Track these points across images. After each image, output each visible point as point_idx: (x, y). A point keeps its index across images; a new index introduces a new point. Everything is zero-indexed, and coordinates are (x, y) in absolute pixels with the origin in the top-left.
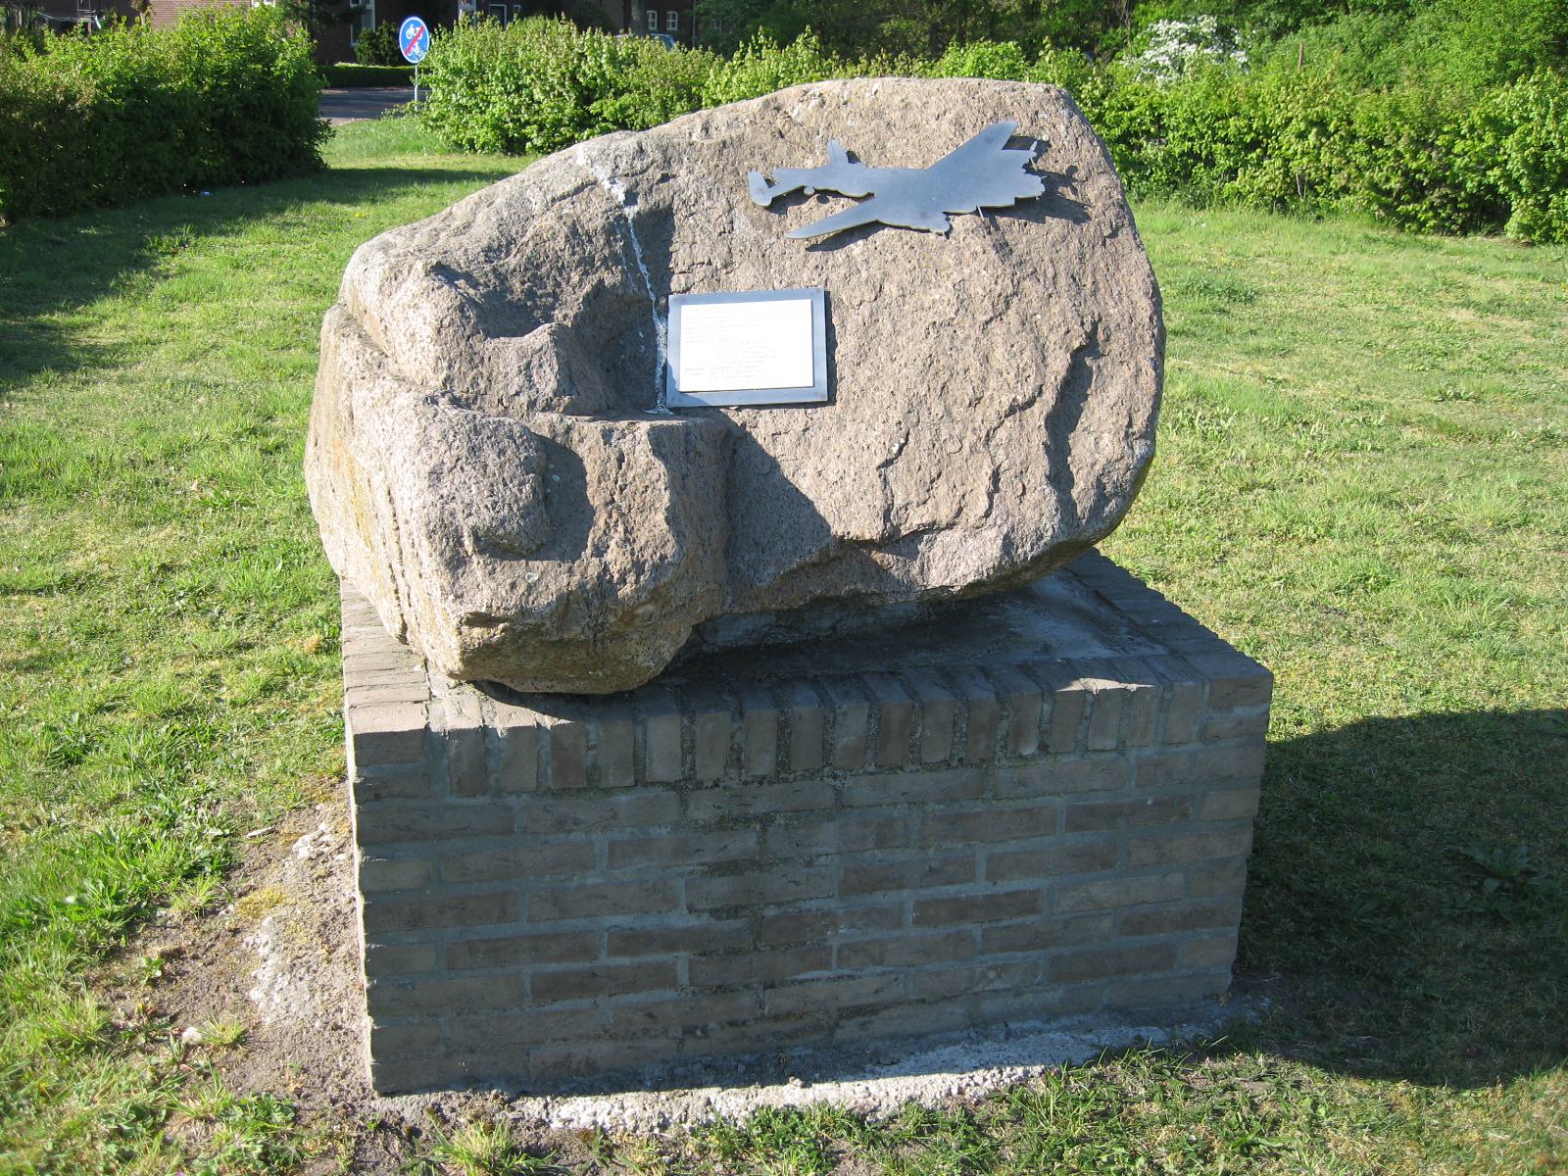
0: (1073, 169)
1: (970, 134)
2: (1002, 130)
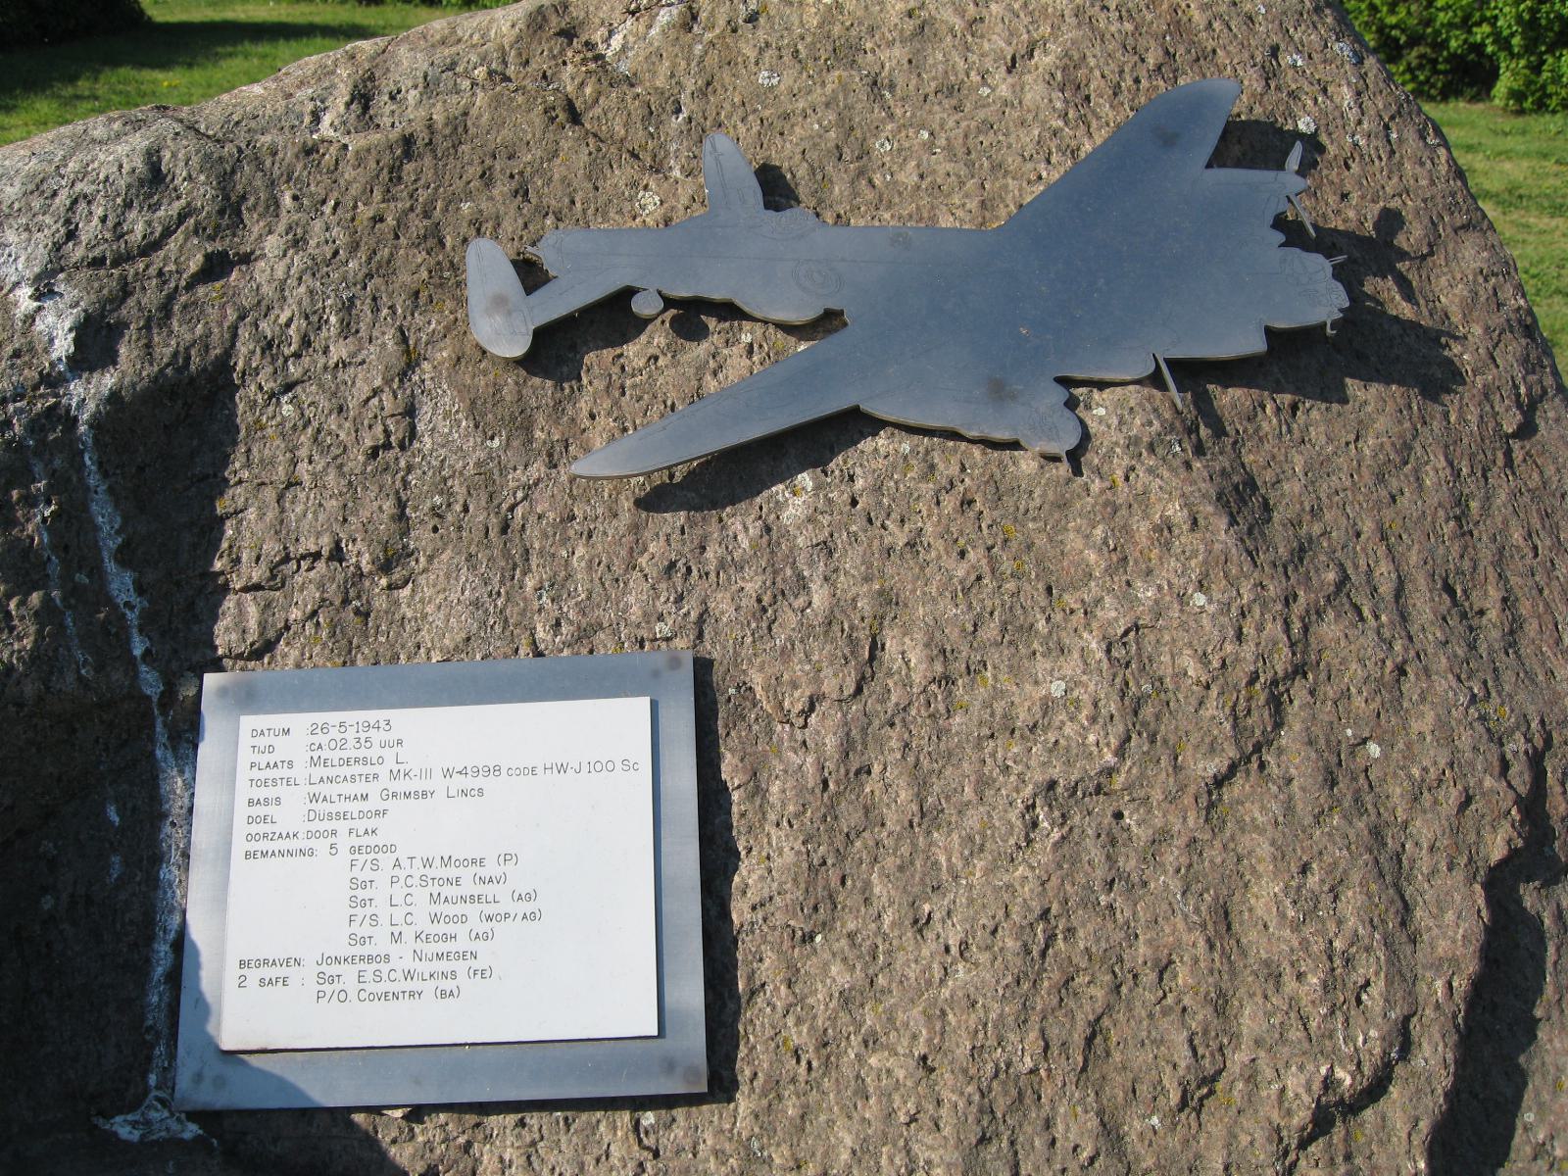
0: (1391, 221)
1: (1109, 115)
2: (1196, 105)
